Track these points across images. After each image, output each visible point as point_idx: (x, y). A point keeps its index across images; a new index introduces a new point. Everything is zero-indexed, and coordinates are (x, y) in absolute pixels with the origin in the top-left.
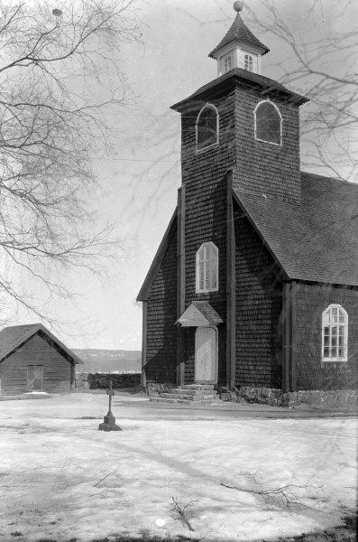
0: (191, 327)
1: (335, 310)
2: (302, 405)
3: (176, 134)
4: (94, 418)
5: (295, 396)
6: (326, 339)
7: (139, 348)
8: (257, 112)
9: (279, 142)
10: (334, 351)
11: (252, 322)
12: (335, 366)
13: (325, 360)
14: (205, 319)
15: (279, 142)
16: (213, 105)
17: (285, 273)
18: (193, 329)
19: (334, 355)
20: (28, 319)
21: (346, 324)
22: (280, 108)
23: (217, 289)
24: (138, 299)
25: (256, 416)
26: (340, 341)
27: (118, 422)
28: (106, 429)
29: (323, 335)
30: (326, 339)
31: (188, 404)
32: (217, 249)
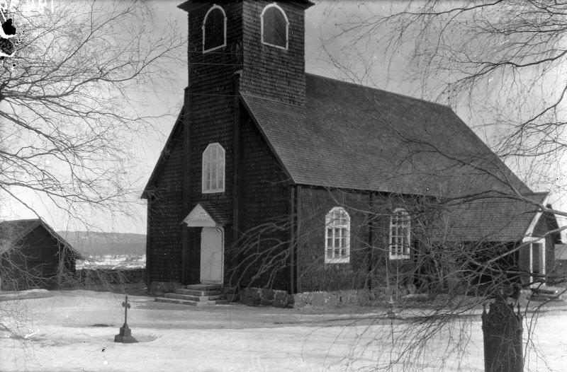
0: (197, 228)
1: (338, 214)
2: (307, 306)
3: (181, 44)
4: (106, 326)
5: (300, 296)
6: (330, 240)
7: (146, 234)
8: (264, 16)
9: (285, 47)
10: (337, 252)
11: (262, 61)
12: (338, 267)
13: (327, 260)
14: (211, 220)
15: (285, 47)
16: (220, 7)
17: (292, 181)
18: (199, 230)
19: (337, 257)
20: (28, 215)
21: (348, 226)
22: (287, 13)
23: (223, 190)
24: (144, 195)
25: (264, 322)
26: (343, 244)
27: (134, 332)
28: (122, 341)
29: (327, 237)
30: (330, 240)
31: (195, 304)
32: (224, 150)
